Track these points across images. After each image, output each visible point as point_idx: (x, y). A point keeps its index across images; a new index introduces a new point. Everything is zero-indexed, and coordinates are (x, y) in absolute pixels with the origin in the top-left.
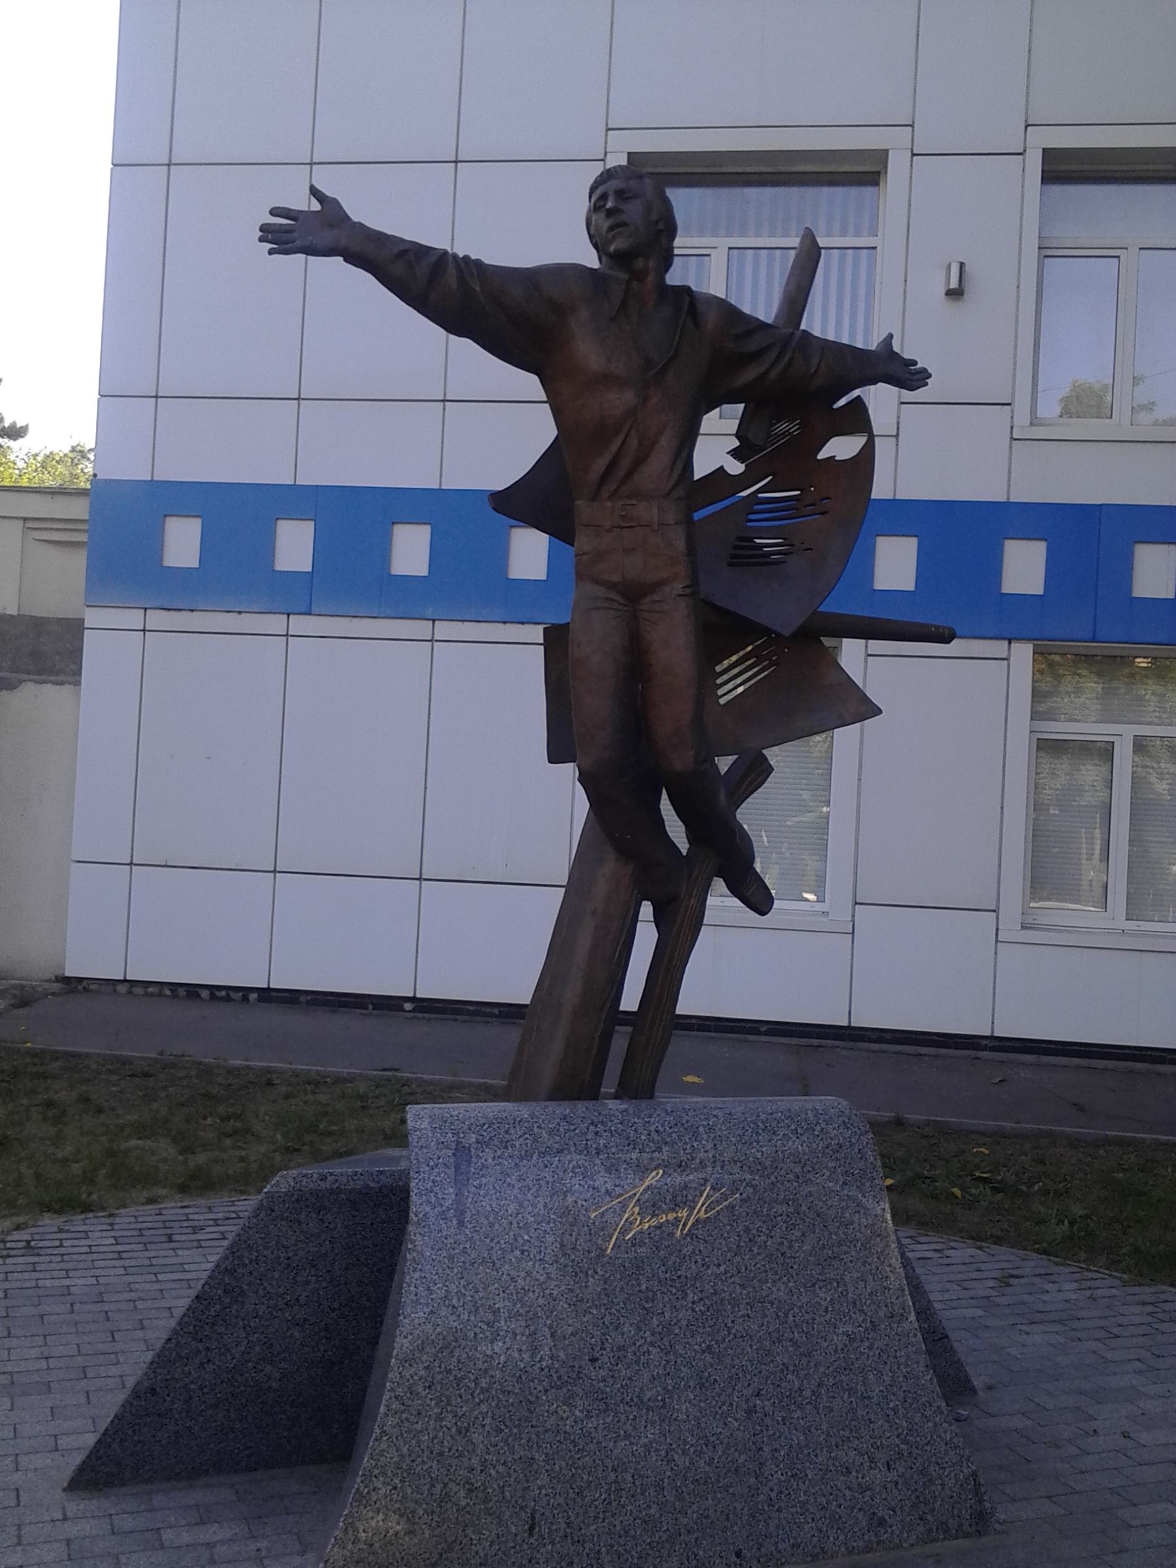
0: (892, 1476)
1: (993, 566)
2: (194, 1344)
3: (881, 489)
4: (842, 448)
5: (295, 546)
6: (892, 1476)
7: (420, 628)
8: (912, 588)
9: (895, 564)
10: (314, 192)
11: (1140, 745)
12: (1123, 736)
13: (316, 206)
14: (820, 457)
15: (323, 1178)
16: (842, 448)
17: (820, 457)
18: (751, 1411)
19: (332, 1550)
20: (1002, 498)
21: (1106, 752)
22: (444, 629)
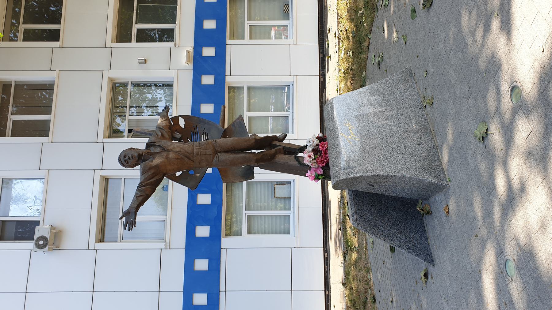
0: (401, 85)
1: (201, 273)
2: (396, 240)
3: (189, 114)
4: (182, 122)
5: (210, 24)
6: (401, 85)
7: (222, 295)
8: (207, 260)
9: (207, 109)
10: (121, 218)
11: (248, 208)
12: (245, 213)
13: (125, 218)
14: (184, 127)
15: (353, 216)
16: (182, 122)
17: (184, 127)
18: (390, 111)
19: (390, 34)
20: (182, 294)
21: (250, 218)
22: (222, 288)
